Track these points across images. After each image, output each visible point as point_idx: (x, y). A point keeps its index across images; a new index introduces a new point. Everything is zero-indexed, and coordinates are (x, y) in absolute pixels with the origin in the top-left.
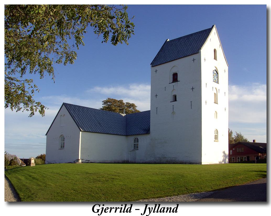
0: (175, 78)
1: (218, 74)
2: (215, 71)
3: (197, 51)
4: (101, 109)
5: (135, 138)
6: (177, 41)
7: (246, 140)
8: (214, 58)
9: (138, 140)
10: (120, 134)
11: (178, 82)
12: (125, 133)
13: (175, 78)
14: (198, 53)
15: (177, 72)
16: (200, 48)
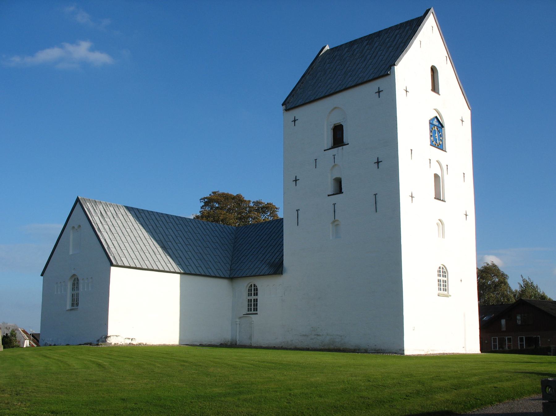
0: (338, 137)
1: (442, 126)
2: (436, 120)
3: (385, 69)
4: (197, 217)
5: (251, 286)
6: (346, 49)
7: (543, 297)
8: (430, 88)
9: (256, 290)
10: (213, 275)
11: (344, 147)
12: (228, 272)
13: (338, 137)
14: (388, 75)
15: (341, 123)
16: (392, 64)
